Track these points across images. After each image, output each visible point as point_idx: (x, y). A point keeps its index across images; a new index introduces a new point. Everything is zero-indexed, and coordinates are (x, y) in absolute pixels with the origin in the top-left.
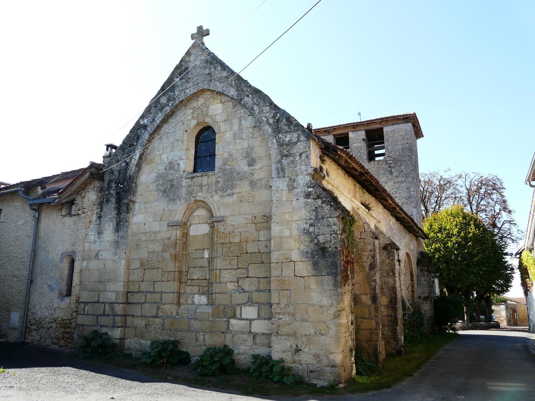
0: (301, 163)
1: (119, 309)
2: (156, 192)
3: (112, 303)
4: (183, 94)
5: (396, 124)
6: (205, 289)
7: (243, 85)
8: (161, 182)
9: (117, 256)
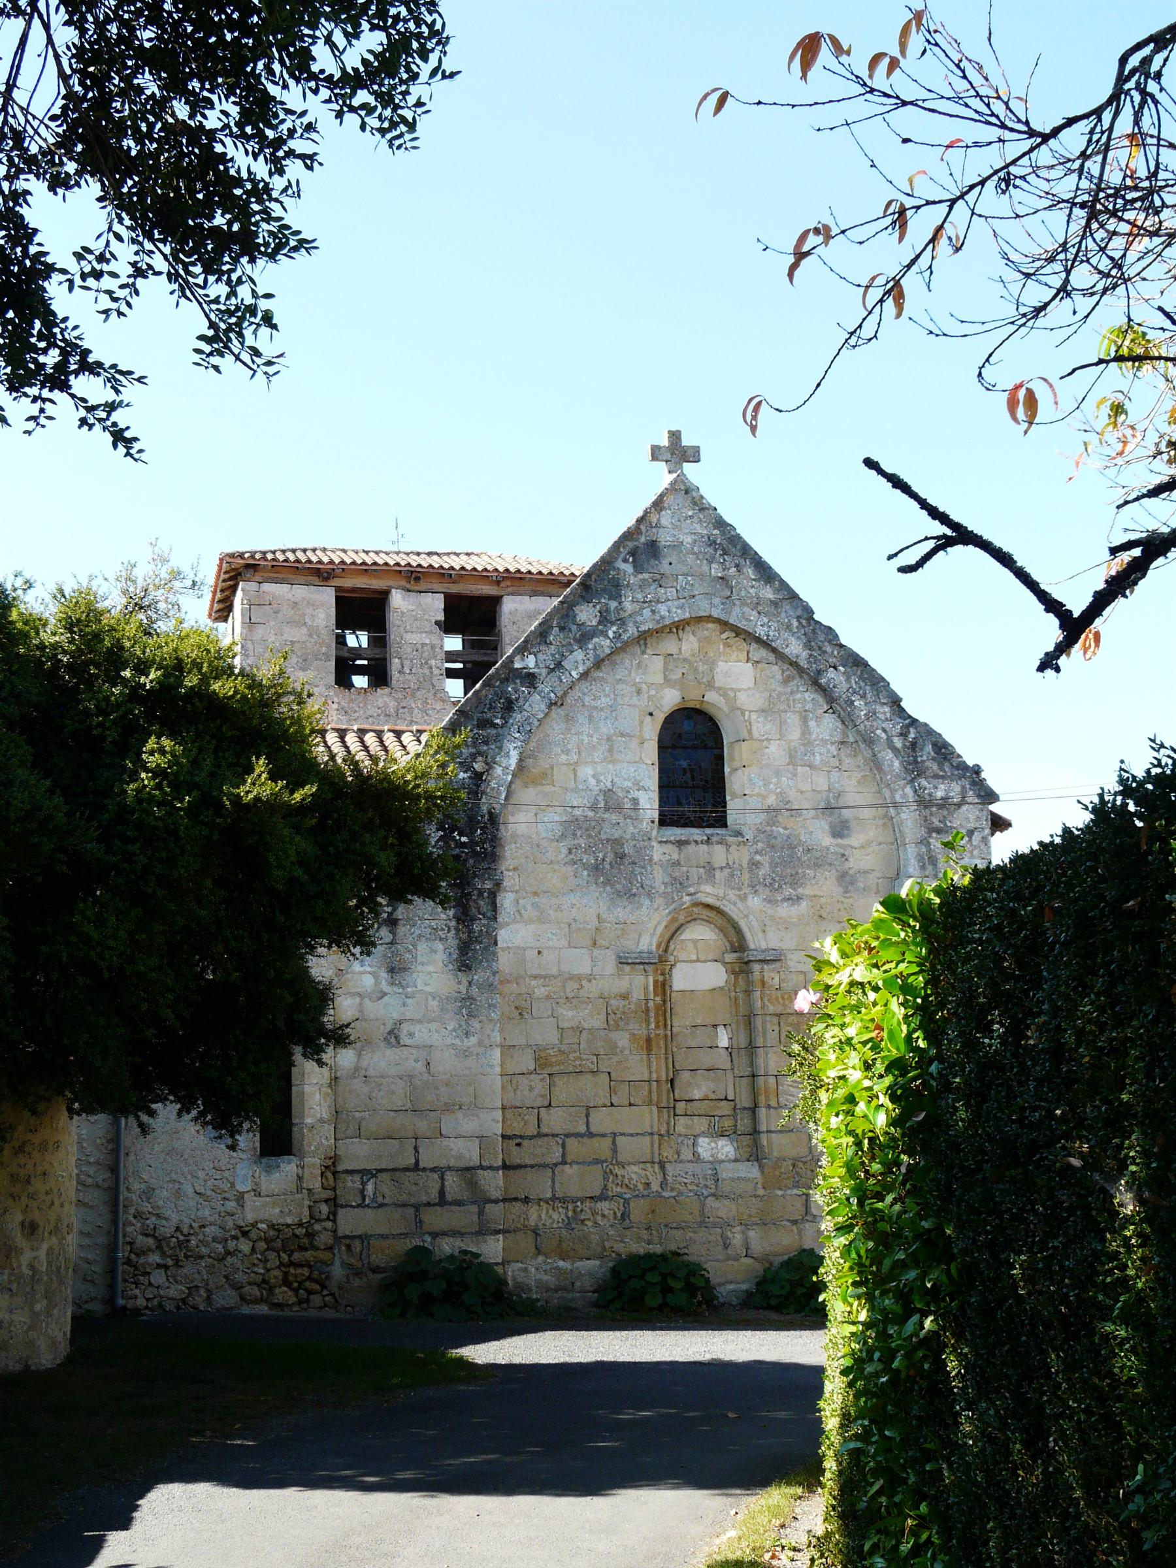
0: (971, 852)
1: (494, 1183)
2: (570, 868)
3: (468, 1169)
4: (647, 612)
5: (542, 594)
6: (727, 1123)
7: (822, 637)
8: (583, 842)
9: (473, 1040)
